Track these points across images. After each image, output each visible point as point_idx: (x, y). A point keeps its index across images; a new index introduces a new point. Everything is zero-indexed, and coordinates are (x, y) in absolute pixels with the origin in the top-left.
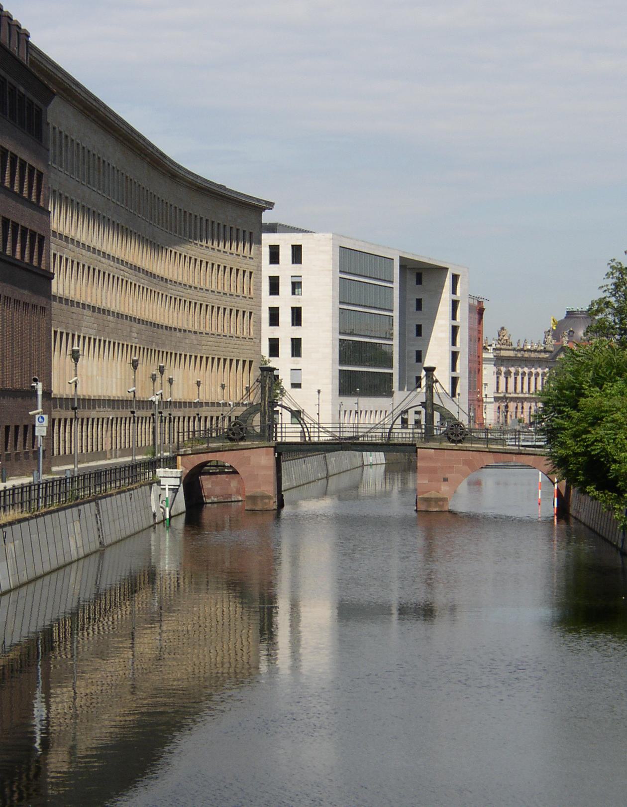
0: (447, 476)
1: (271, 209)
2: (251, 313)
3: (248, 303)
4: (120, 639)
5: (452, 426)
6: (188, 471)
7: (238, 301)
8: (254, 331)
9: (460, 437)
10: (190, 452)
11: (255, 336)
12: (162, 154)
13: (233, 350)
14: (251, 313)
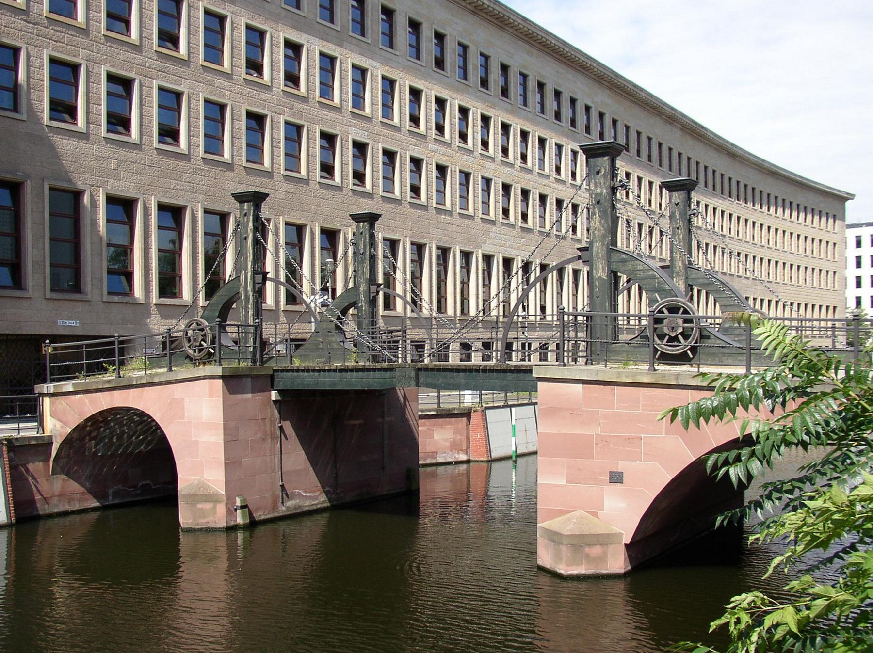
0: (621, 466)
1: (852, 199)
2: (835, 273)
3: (831, 264)
4: (411, 622)
5: (661, 312)
6: (70, 430)
7: (821, 263)
8: (838, 285)
9: (684, 345)
10: (71, 389)
11: (839, 289)
12: (635, 86)
13: (785, 291)
14: (835, 273)
